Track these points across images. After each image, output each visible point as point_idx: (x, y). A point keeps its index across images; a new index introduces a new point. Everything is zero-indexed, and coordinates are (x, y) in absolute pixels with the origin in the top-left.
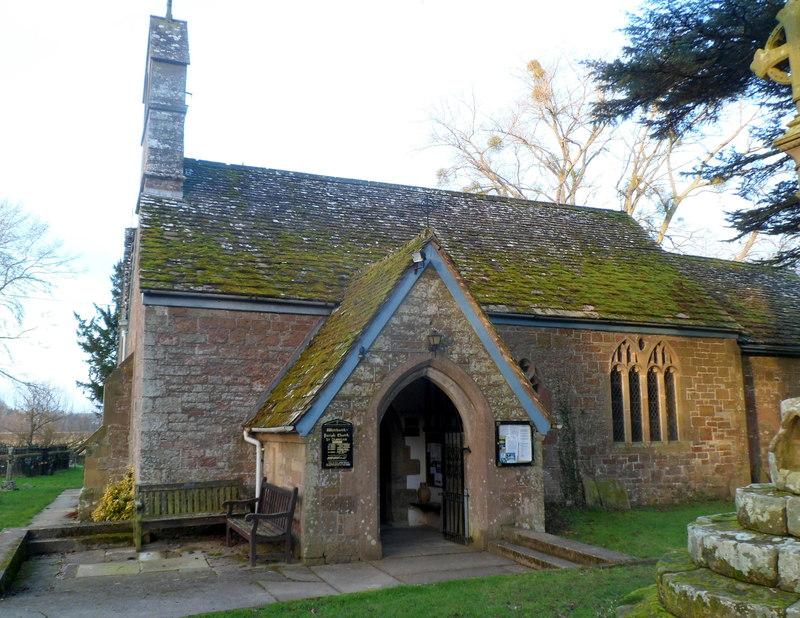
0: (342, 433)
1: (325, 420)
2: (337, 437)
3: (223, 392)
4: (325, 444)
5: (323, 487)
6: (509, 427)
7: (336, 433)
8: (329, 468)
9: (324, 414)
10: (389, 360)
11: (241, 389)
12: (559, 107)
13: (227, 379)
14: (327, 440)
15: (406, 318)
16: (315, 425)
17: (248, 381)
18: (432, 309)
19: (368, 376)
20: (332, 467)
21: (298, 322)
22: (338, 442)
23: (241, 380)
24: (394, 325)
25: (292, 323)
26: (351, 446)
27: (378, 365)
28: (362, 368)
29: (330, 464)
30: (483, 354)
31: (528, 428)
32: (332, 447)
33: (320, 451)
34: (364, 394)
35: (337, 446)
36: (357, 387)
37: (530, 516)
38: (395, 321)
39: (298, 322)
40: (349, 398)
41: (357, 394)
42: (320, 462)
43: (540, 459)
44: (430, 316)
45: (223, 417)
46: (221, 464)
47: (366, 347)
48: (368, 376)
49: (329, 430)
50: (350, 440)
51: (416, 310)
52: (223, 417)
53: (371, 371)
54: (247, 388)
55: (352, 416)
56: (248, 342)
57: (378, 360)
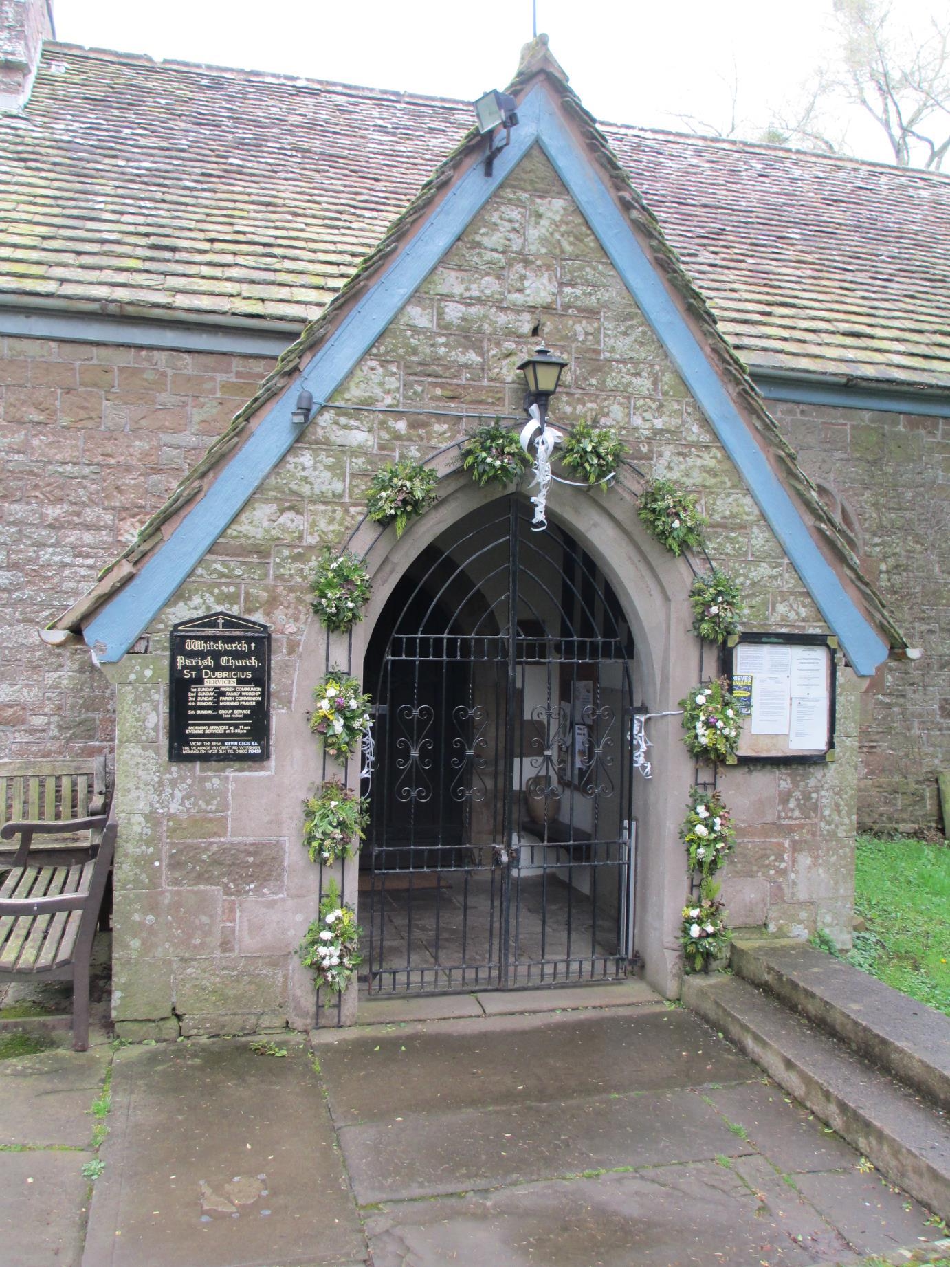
0: (237, 655)
1: (182, 612)
2: (218, 668)
3: (42, 545)
4: (180, 688)
5: (171, 817)
6: (765, 653)
7: (216, 655)
8: (191, 758)
9: (179, 595)
10: (397, 436)
11: (88, 537)
12: (896, 75)
13: (53, 512)
14: (187, 675)
15: (453, 312)
16: (149, 629)
17: (108, 518)
18: (539, 288)
19: (326, 482)
20: (204, 758)
21: (238, 374)
22: (226, 682)
23: (90, 515)
24: (416, 330)
25: (220, 377)
26: (266, 695)
27: (360, 451)
28: (306, 459)
29: (195, 749)
30: (695, 431)
31: (819, 656)
32: (201, 696)
33: (164, 709)
34: (311, 540)
35: (219, 693)
36: (290, 515)
37: (811, 904)
38: (419, 316)
39: (238, 374)
40: (260, 551)
41: (288, 538)
42: (164, 741)
43: (848, 741)
44: (532, 309)
45: (43, 606)
46: (39, 721)
47: (319, 398)
48: (326, 482)
49: (191, 645)
50: (260, 678)
51: (490, 285)
52: (43, 606)
53: (337, 470)
54: (105, 536)
55: (272, 603)
56: (108, 423)
57: (359, 437)
